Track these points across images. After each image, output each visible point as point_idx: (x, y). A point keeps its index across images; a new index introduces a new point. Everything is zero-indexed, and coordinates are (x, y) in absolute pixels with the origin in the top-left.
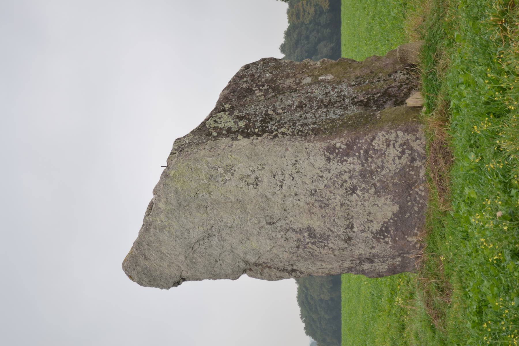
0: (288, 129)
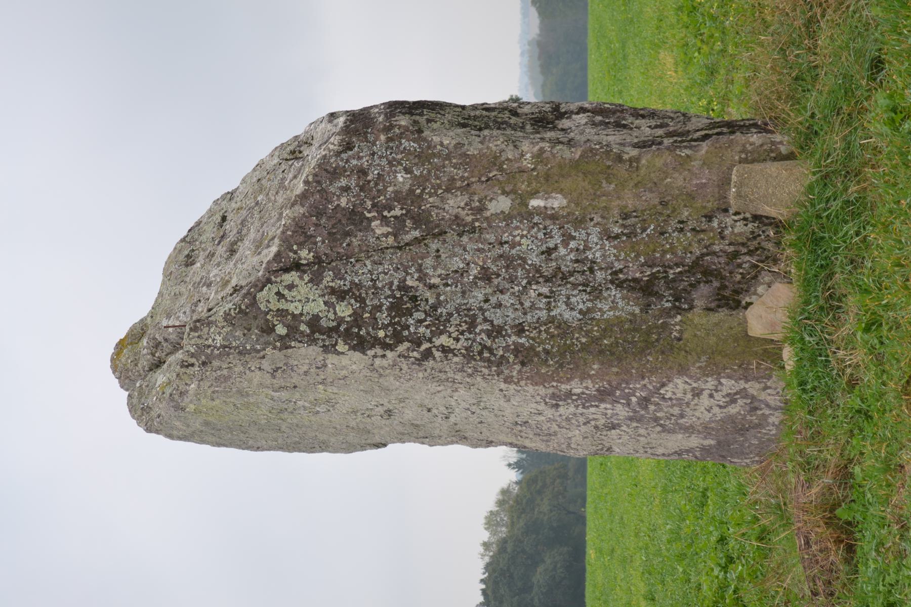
0: (457, 340)
